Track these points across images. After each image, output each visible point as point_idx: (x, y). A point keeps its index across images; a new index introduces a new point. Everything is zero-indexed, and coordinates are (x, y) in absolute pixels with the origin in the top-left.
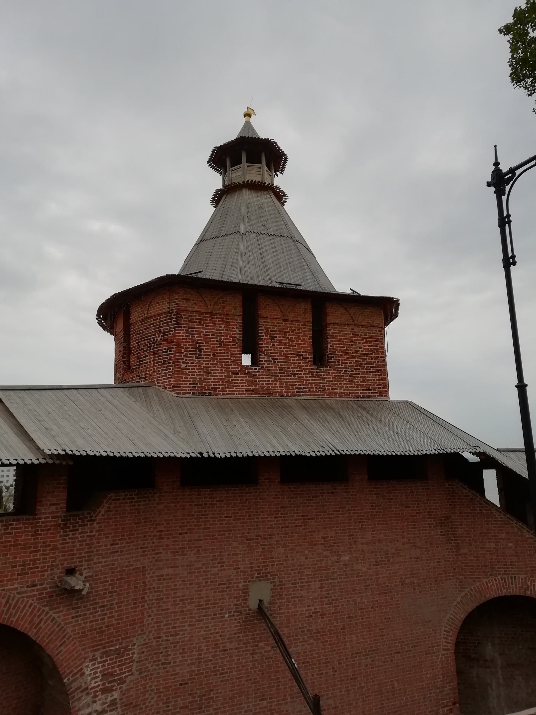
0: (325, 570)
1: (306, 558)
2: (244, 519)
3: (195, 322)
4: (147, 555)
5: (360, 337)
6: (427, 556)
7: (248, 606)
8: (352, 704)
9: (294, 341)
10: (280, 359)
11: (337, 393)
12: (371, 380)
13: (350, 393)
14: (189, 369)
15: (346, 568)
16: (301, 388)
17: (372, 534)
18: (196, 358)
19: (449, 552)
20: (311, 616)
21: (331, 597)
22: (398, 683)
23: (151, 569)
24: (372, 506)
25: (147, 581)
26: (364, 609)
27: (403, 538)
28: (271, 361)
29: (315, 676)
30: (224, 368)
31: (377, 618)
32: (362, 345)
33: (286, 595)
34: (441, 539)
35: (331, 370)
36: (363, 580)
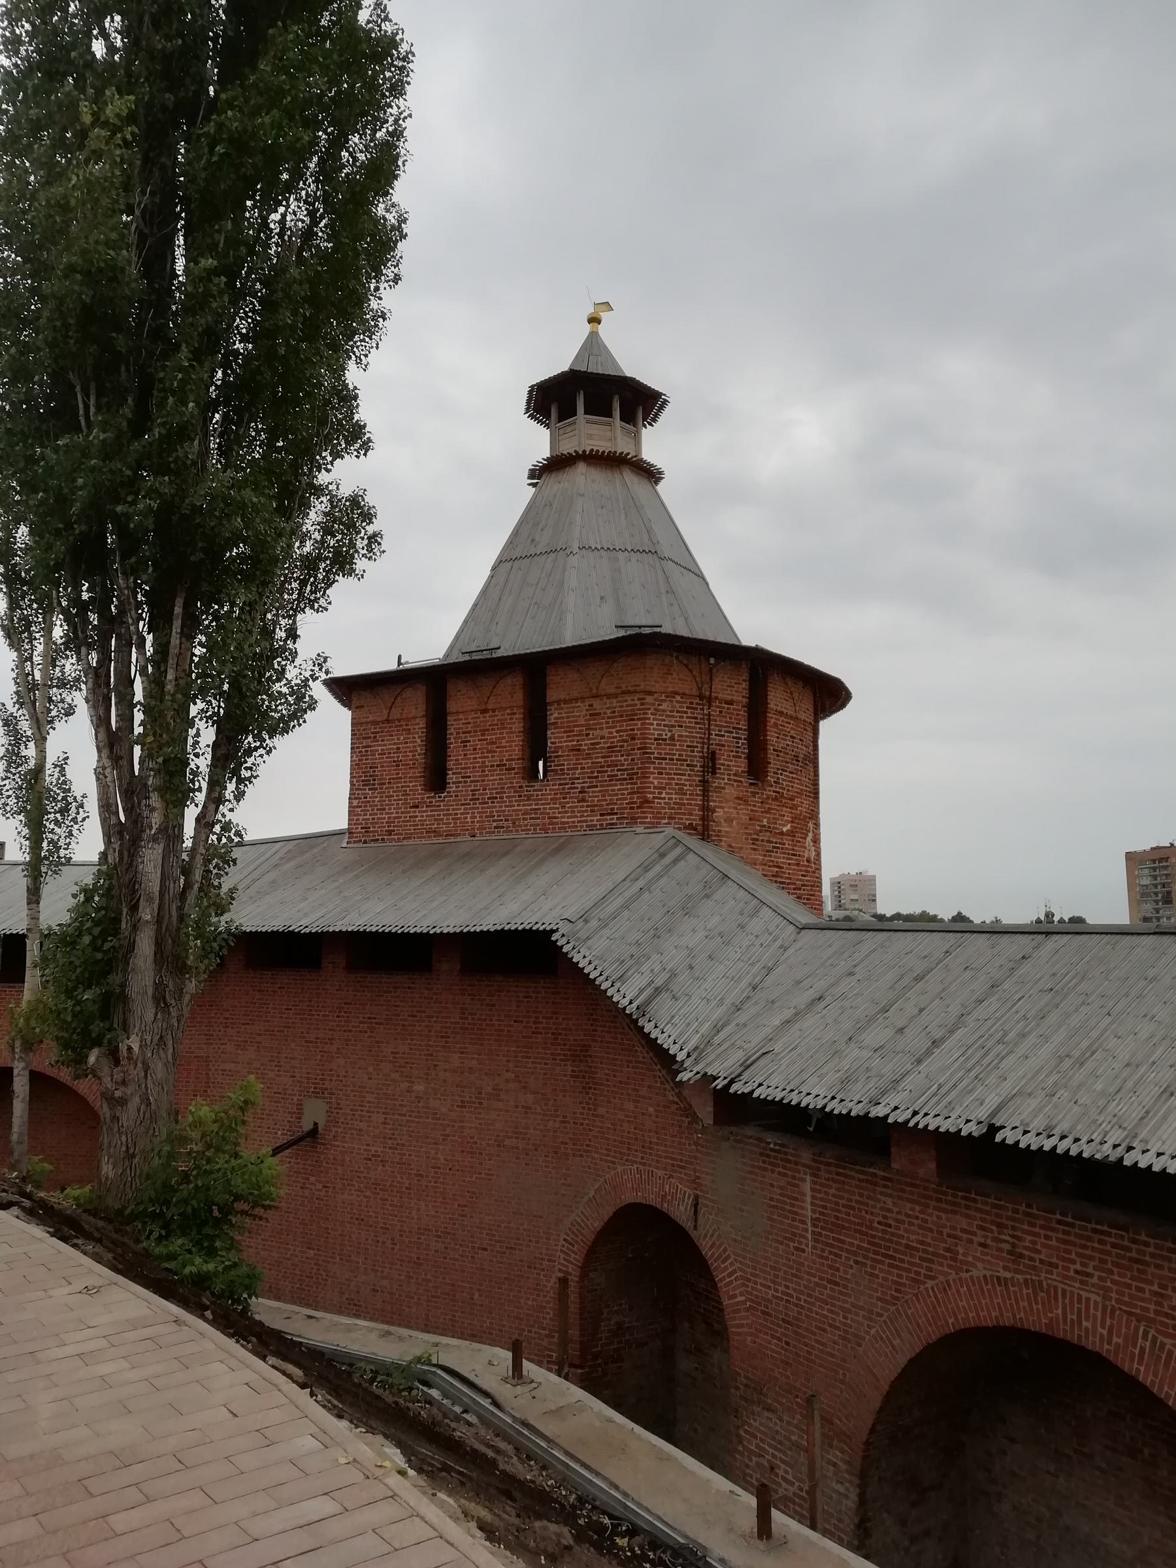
0: (392, 1100)
1: (370, 1079)
2: (304, 1014)
3: (370, 738)
4: (212, 1044)
5: (603, 718)
6: (545, 1107)
7: (301, 1127)
8: (412, 1298)
9: (495, 743)
10: (474, 776)
11: (557, 823)
12: (616, 795)
13: (578, 822)
14: (361, 807)
15: (419, 1102)
16: (501, 820)
17: (460, 1058)
18: (370, 789)
19: (584, 1108)
20: (370, 1160)
21: (396, 1139)
22: (480, 1296)
23: (216, 1061)
24: (464, 1013)
25: (211, 1073)
26: (439, 1168)
27: (507, 1071)
28: (460, 782)
29: (370, 1241)
30: (401, 800)
31: (456, 1187)
32: (605, 732)
33: (343, 1123)
34: (572, 1083)
35: (549, 785)
36: (441, 1124)
